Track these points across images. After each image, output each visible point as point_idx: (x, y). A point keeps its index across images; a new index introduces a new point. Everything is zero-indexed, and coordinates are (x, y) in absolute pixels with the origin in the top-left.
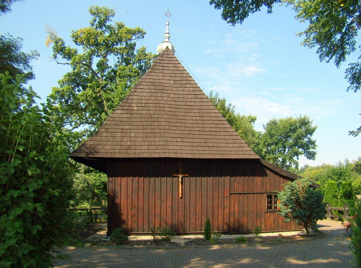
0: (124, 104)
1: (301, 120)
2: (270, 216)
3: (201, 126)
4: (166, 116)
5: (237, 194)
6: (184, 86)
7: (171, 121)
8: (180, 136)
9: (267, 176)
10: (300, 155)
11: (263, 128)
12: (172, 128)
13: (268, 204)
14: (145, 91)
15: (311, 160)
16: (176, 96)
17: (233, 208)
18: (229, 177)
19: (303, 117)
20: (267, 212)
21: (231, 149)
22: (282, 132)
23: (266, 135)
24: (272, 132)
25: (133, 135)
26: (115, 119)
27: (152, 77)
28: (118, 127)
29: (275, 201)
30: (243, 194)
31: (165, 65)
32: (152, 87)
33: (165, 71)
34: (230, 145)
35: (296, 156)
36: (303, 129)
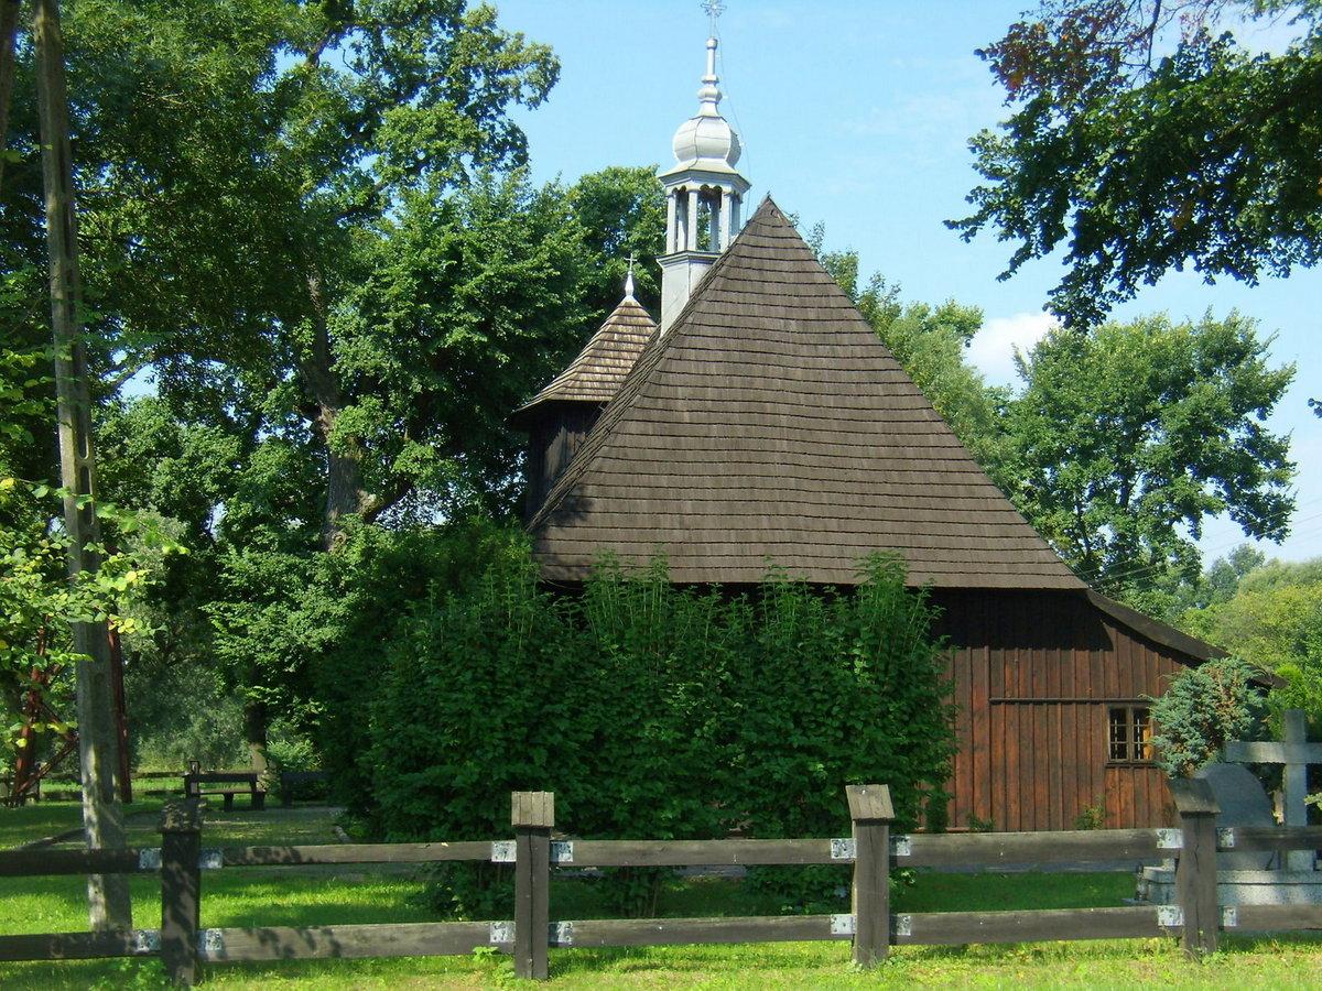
0: (647, 403)
1: (1210, 338)
2: (1120, 780)
3: (895, 476)
4: (785, 445)
5: (1013, 703)
6: (831, 339)
7: (804, 460)
8: (835, 511)
9: (1108, 646)
10: (1206, 518)
11: (1013, 367)
12: (806, 485)
13: (1113, 739)
14: (711, 356)
15: (1265, 539)
16: (811, 375)
17: (1001, 752)
18: (986, 648)
19: (1219, 319)
20: (1111, 766)
21: (996, 556)
22: (1115, 396)
23: (1033, 408)
24: (1065, 394)
25: (688, 507)
26: (626, 454)
27: (730, 308)
28: (637, 480)
29: (1136, 729)
30: (1031, 706)
31: (768, 265)
32: (732, 344)
33: (768, 288)
34: (990, 543)
35: (1184, 519)
36: (1223, 379)
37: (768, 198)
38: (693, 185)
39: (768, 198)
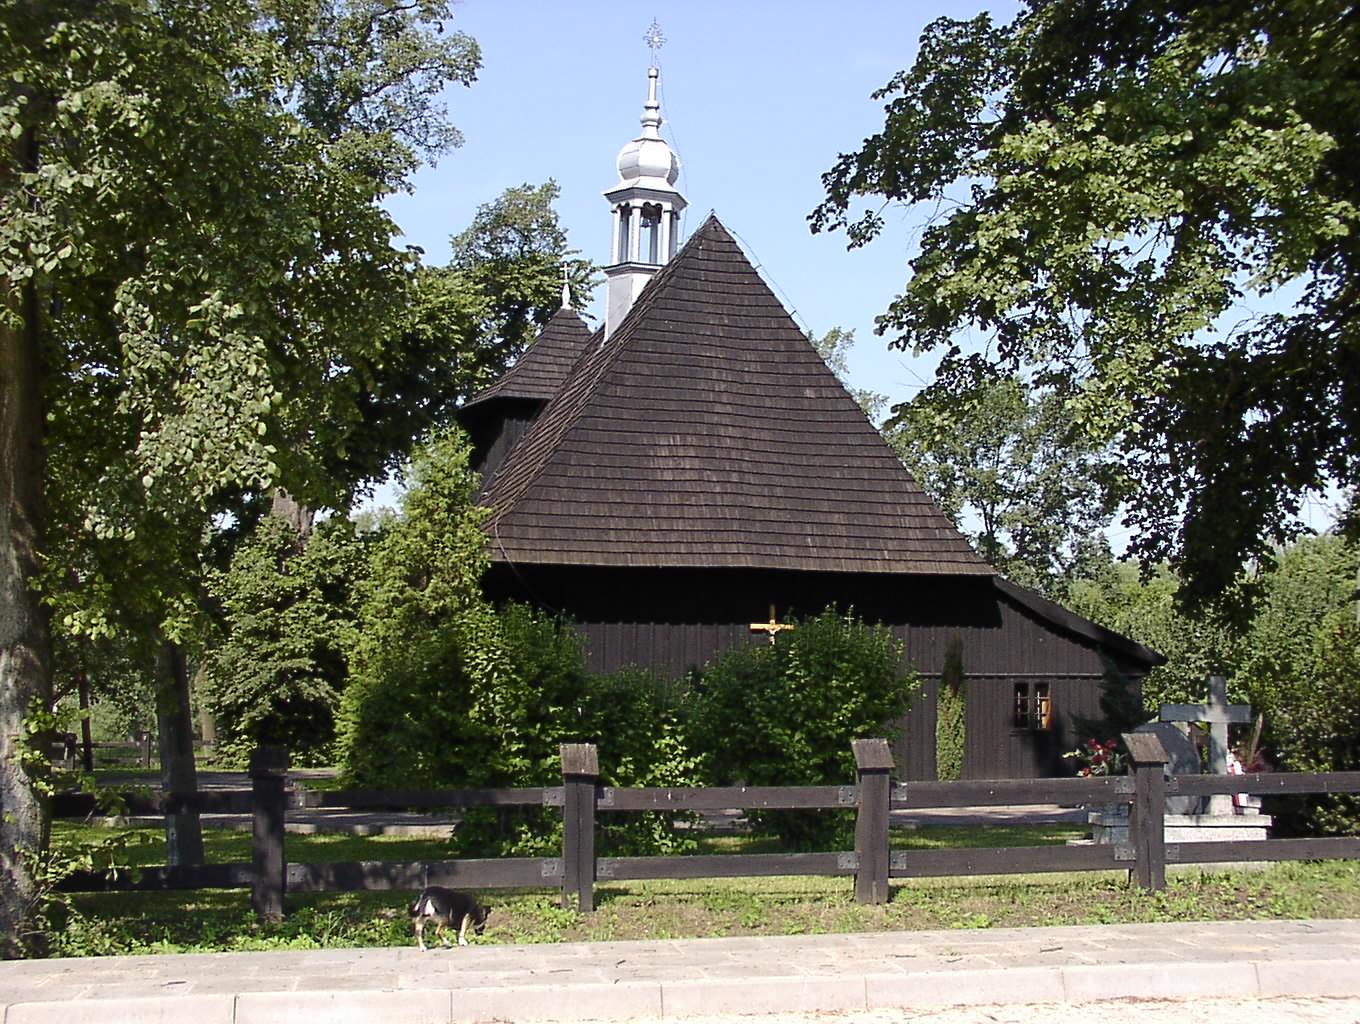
9: (998, 623)
18: (907, 626)
37: (713, 217)
38: (639, 202)
39: (713, 217)
